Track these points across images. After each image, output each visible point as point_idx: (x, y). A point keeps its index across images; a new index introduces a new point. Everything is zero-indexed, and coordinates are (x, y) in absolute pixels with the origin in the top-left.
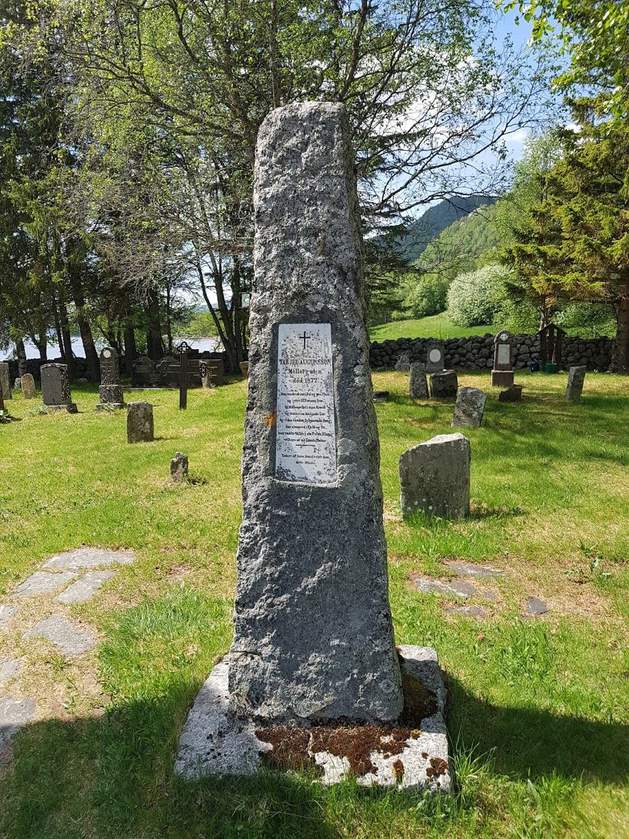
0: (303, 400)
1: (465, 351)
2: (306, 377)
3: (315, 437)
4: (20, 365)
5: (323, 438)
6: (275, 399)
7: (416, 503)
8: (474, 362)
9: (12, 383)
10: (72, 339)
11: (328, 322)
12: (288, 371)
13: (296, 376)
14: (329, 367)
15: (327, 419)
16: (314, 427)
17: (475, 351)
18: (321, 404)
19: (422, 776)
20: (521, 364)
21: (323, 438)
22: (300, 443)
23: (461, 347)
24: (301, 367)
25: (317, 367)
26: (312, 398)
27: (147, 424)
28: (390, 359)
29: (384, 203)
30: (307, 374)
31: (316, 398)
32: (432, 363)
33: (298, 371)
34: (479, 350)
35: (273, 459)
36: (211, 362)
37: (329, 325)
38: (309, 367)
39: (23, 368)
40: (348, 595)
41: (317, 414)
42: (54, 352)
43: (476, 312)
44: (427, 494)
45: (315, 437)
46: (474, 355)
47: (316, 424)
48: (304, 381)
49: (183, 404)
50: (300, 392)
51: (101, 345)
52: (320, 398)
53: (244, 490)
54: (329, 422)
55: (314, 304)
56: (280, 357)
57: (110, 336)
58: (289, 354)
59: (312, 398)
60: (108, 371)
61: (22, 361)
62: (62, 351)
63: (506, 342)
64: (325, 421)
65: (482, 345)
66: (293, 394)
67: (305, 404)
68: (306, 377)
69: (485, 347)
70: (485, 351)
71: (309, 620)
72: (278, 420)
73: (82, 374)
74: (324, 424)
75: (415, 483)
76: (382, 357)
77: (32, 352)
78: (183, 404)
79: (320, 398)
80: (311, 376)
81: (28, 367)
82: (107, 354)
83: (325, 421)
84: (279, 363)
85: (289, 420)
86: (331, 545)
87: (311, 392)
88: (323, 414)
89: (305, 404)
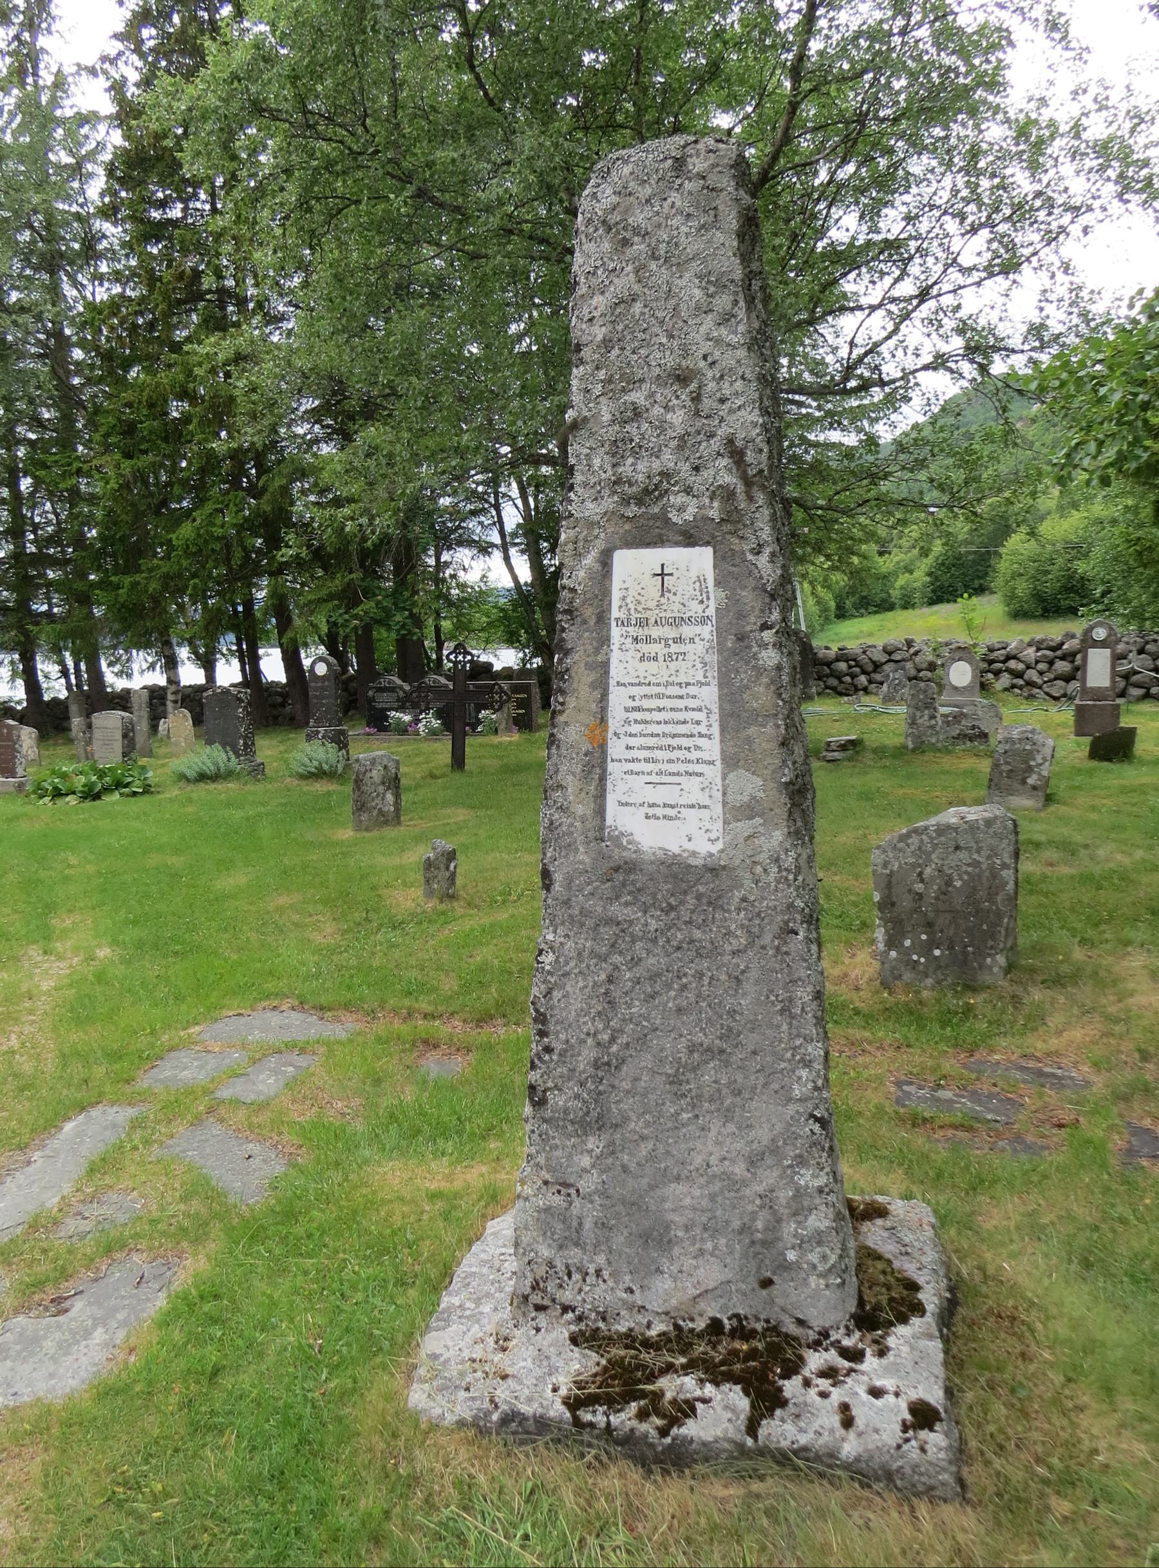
0: (658, 696)
1: (1021, 666)
2: (666, 650)
3: (681, 767)
4: (170, 697)
5: (698, 768)
6: (605, 696)
7: (908, 943)
8: (1040, 688)
9: (154, 728)
10: (261, 652)
11: (707, 544)
12: (630, 640)
13: (645, 648)
14: (707, 631)
15: (704, 731)
16: (680, 748)
17: (1042, 666)
18: (692, 703)
19: (891, 1433)
20: (1136, 692)
21: (698, 768)
22: (654, 778)
23: (1015, 657)
24: (656, 632)
25: (687, 631)
26: (675, 690)
27: (390, 797)
28: (870, 682)
29: (849, 370)
30: (667, 645)
31: (683, 692)
32: (956, 688)
33: (649, 640)
34: (1051, 663)
35: (601, 812)
36: (516, 685)
37: (708, 552)
38: (670, 633)
39: (175, 702)
40: (746, 1077)
41: (685, 722)
42: (229, 673)
43: (1049, 587)
44: (930, 925)
45: (681, 767)
46: (1041, 673)
47: (685, 742)
48: (661, 659)
49: (458, 760)
50: (653, 680)
51: (314, 659)
52: (692, 690)
53: (546, 874)
54: (709, 737)
55: (681, 509)
56: (615, 613)
57: (331, 642)
58: (632, 606)
59: (675, 690)
60: (327, 700)
61: (173, 688)
62: (243, 670)
63: (1103, 644)
64: (701, 735)
65: (1059, 653)
66: (640, 684)
67: (661, 703)
68: (666, 650)
69: (1063, 658)
70: (1062, 666)
71: (670, 1125)
72: (610, 735)
73: (272, 709)
74: (701, 742)
75: (906, 903)
76: (853, 676)
77: (191, 675)
78: (458, 760)
79: (692, 690)
80: (674, 648)
81: (183, 700)
82: (321, 669)
83: (701, 735)
84: (614, 624)
85: (631, 735)
86: (712, 978)
87: (673, 678)
88: (698, 723)
89: (661, 703)
